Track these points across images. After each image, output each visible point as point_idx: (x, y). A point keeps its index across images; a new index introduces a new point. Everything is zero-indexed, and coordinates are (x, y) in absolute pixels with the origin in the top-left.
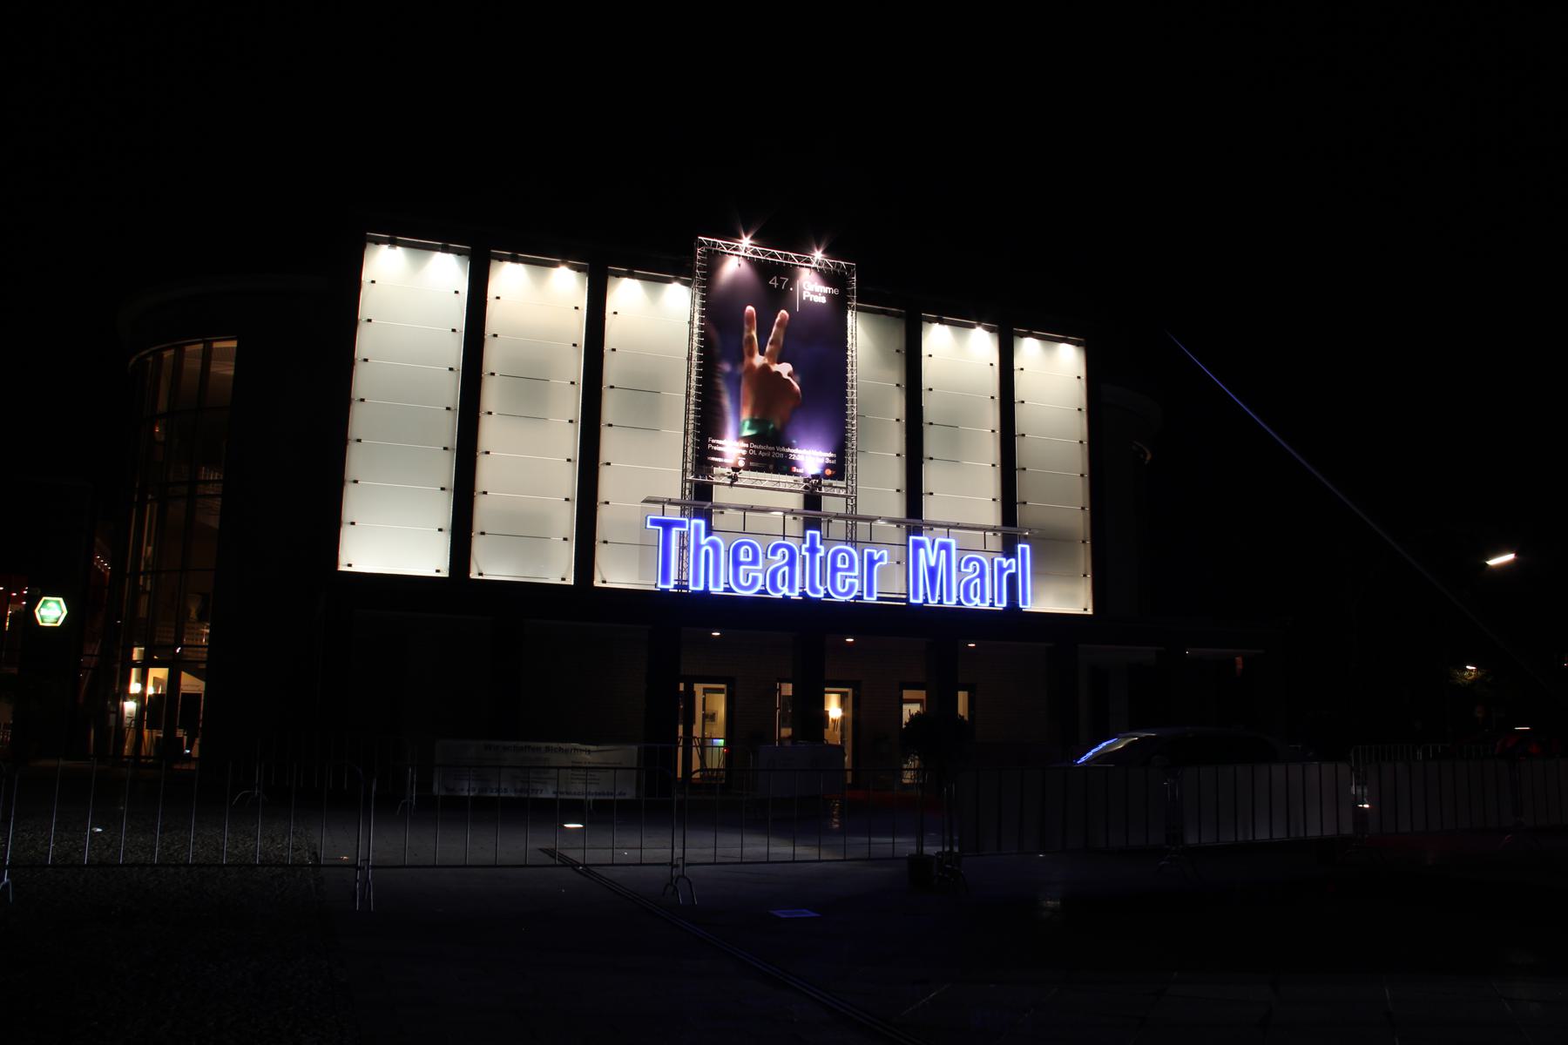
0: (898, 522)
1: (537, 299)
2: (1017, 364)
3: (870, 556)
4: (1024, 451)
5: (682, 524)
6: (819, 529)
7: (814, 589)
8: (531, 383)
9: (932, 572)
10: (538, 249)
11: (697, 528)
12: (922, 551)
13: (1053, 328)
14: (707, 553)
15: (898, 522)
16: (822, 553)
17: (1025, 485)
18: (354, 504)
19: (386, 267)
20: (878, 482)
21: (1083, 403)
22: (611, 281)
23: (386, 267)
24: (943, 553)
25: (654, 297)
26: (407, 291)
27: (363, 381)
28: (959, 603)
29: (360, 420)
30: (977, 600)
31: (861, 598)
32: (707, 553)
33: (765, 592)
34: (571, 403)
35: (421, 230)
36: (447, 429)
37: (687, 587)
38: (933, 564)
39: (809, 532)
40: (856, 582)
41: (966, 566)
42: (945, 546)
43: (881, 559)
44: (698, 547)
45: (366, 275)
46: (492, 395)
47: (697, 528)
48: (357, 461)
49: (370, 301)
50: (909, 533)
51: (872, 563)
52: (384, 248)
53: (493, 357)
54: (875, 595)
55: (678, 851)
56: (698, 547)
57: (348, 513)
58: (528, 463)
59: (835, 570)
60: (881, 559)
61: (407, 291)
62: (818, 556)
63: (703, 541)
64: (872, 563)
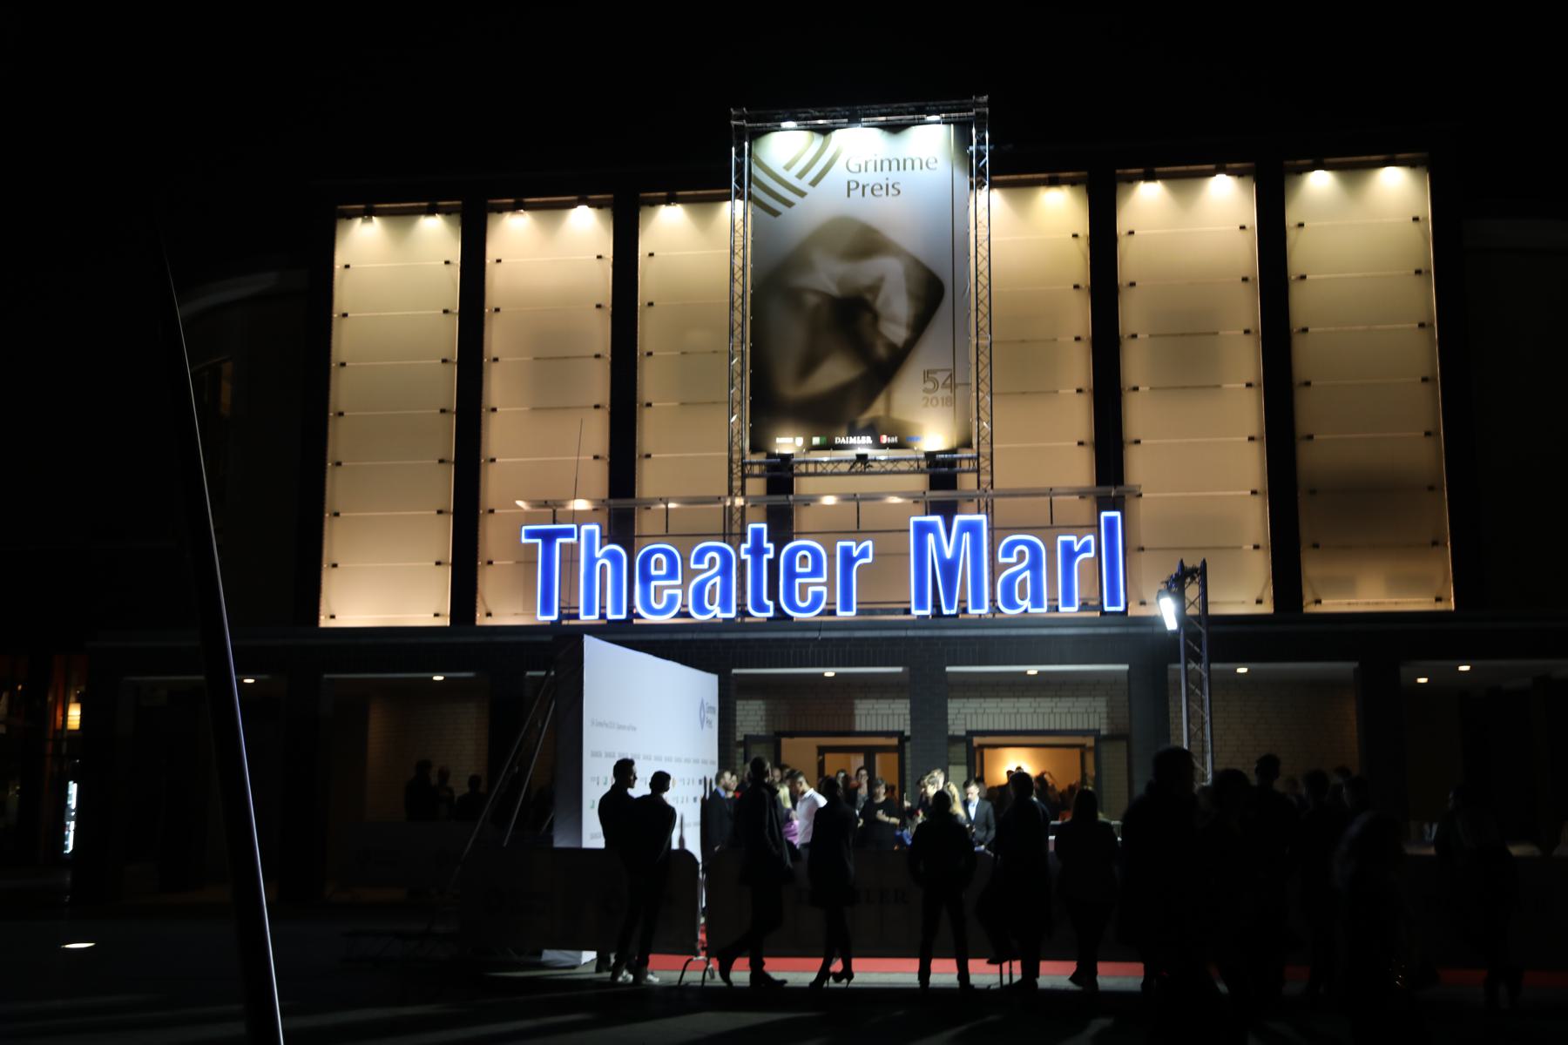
0: (1082, 494)
1: (550, 251)
3: (847, 552)
4: (1306, 357)
5: (569, 533)
9: (949, 568)
10: (547, 191)
11: (590, 535)
12: (931, 538)
13: (1354, 155)
14: (603, 567)
15: (1082, 494)
16: (771, 555)
17: (1308, 409)
18: (336, 542)
19: (364, 243)
20: (1047, 442)
22: (643, 215)
23: (364, 243)
24: (967, 536)
25: (1021, 208)
26: (389, 263)
27: (344, 390)
29: (340, 440)
30: (1026, 604)
32: (603, 567)
33: (687, 615)
35: (399, 197)
39: (1104, 514)
40: (679, 592)
43: (864, 554)
44: (592, 560)
45: (340, 259)
46: (1135, 365)
47: (590, 535)
48: (338, 487)
51: (1069, 554)
53: (1132, 314)
56: (592, 560)
58: (542, 452)
60: (864, 554)
61: (389, 263)
62: (766, 557)
63: (598, 553)
64: (848, 559)
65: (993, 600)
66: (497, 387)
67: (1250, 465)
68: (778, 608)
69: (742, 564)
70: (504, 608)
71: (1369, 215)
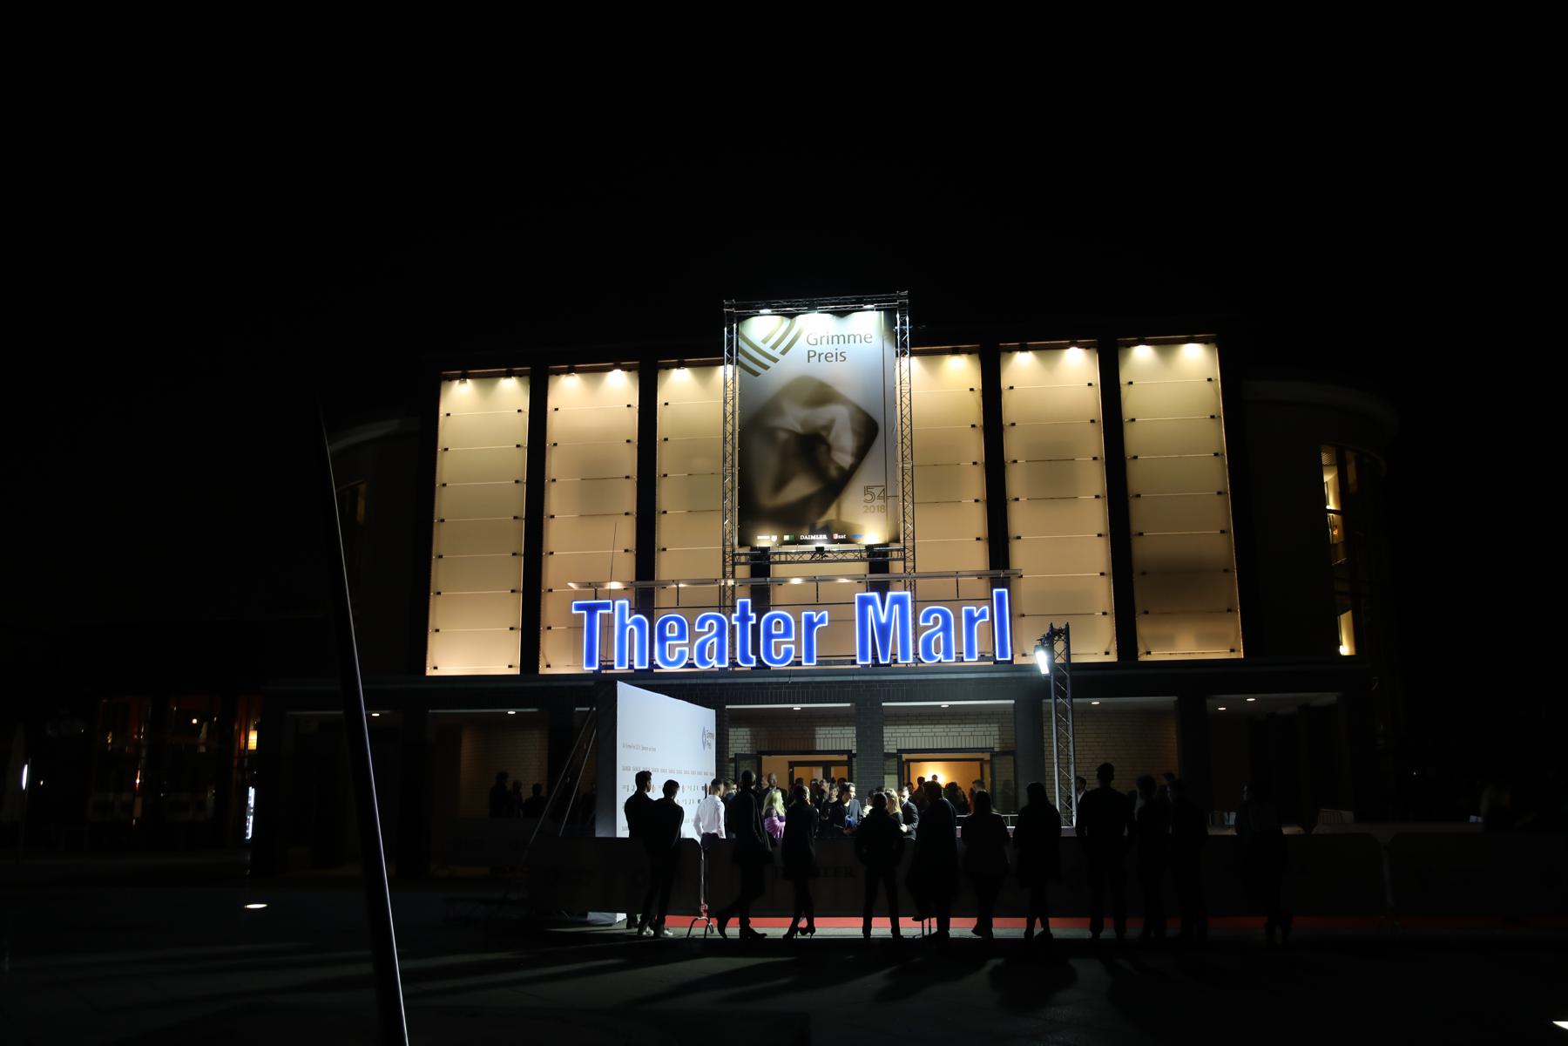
0: (980, 576)
1: (594, 401)
2: (1124, 378)
4: (1137, 476)
5: (606, 606)
6: (1008, 587)
7: (746, 659)
8: (1054, 463)
9: (884, 630)
12: (870, 608)
13: (1166, 334)
15: (980, 576)
17: (1140, 514)
18: (440, 614)
19: (461, 399)
21: (1218, 405)
23: (461, 399)
24: (896, 607)
25: (704, 381)
26: (478, 412)
27: (444, 504)
28: (734, 664)
29: (442, 539)
30: (940, 656)
31: (799, 663)
33: (693, 666)
34: (975, 484)
35: (484, 363)
36: (516, 538)
37: (612, 667)
38: (883, 619)
41: (926, 619)
42: (900, 601)
43: (822, 620)
44: (623, 626)
46: (1017, 482)
48: (440, 574)
49: (447, 432)
50: (994, 586)
51: (971, 620)
52: (675, 371)
53: (1013, 446)
54: (977, 655)
55: (1038, 930)
56: (623, 626)
57: (433, 622)
58: (588, 547)
59: (769, 636)
60: (822, 620)
61: (478, 412)
63: (628, 621)
64: (810, 624)
65: (916, 654)
66: (555, 500)
67: (1098, 554)
68: (759, 660)
69: (733, 628)
70: (559, 662)
71: (1177, 378)
